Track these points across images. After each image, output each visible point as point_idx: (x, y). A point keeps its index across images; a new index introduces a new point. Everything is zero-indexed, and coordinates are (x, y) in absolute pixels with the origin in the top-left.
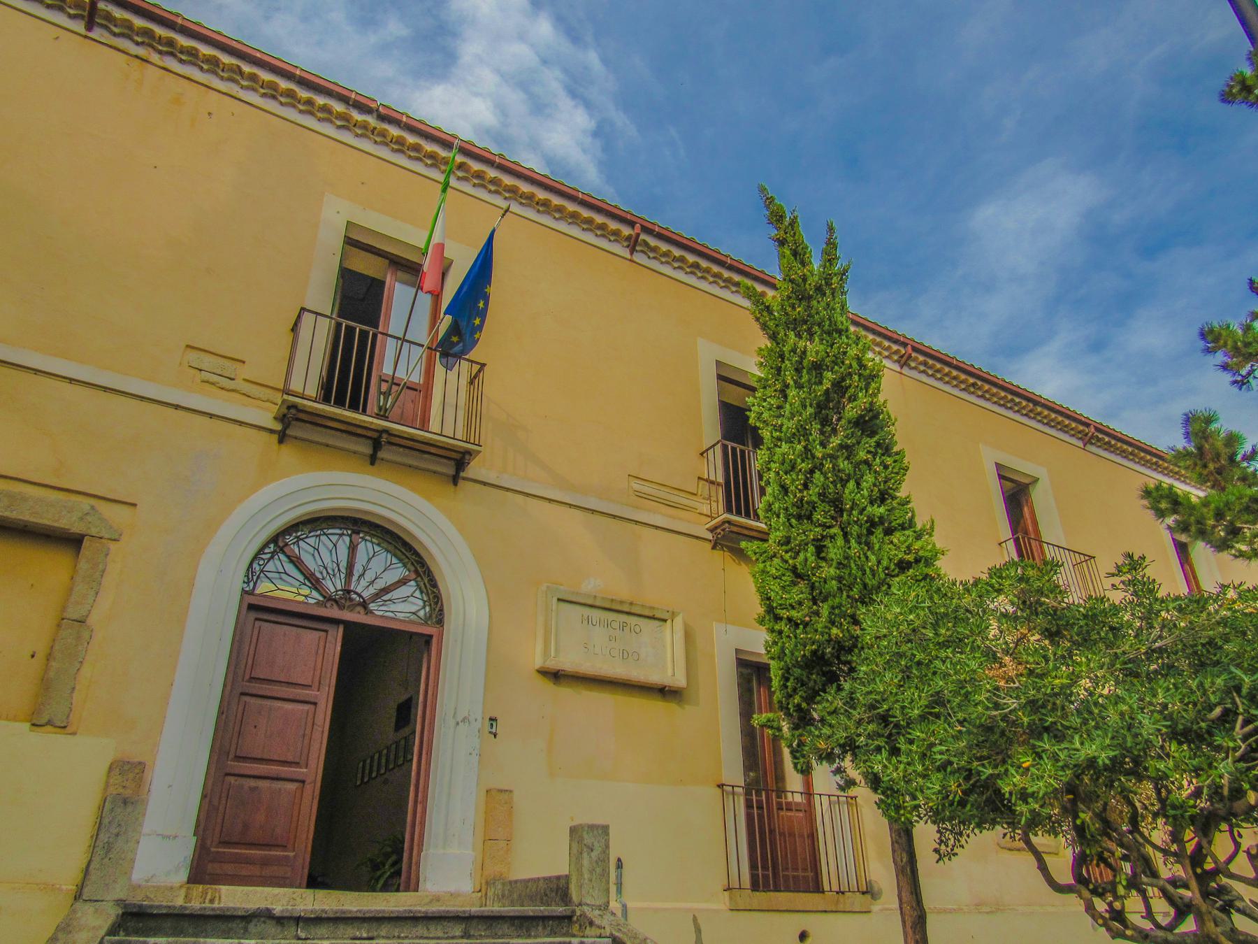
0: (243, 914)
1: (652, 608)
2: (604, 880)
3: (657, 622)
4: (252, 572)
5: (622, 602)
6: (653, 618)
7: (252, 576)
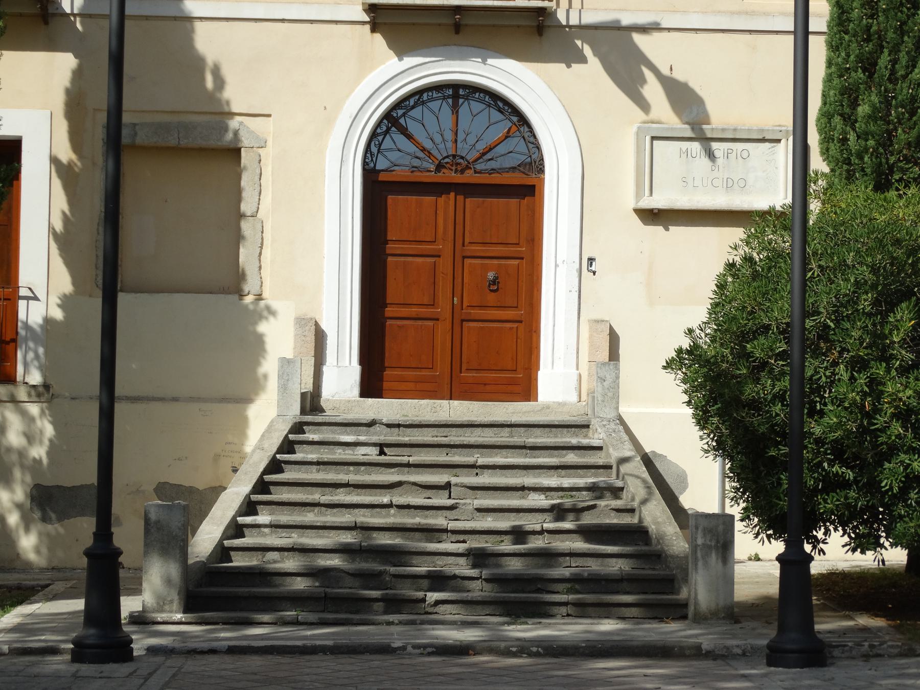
0: (366, 422)
1: (762, 130)
2: (614, 401)
3: (767, 144)
4: (371, 155)
5: (723, 130)
6: (763, 140)
7: (372, 157)
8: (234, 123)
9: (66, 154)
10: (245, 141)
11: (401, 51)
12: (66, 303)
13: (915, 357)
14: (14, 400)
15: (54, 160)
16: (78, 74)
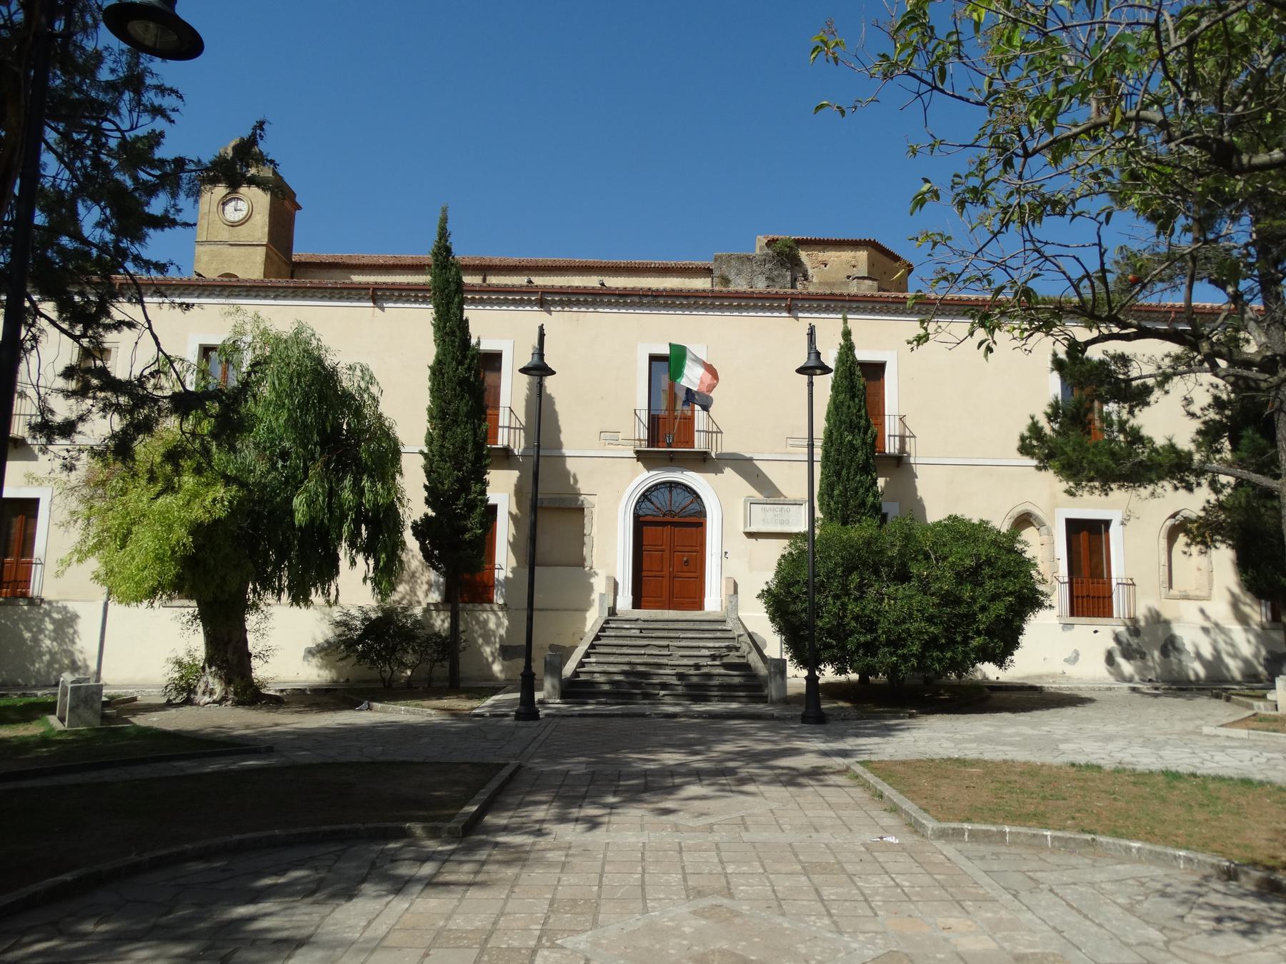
8: (582, 498)
9: (515, 511)
10: (586, 505)
11: (649, 470)
12: (514, 570)
15: (510, 513)
16: (520, 479)
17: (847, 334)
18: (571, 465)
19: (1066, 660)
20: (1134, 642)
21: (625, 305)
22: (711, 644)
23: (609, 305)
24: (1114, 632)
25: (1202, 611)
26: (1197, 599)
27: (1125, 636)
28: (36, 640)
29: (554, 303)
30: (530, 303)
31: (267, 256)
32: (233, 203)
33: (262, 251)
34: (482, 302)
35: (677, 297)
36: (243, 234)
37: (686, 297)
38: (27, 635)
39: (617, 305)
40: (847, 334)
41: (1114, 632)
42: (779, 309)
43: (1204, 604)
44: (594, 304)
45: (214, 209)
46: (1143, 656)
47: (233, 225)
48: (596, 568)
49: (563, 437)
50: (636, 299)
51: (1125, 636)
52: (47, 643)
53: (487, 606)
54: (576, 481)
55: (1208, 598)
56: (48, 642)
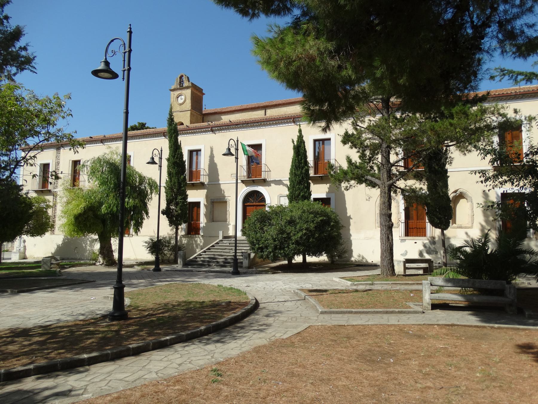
8: (226, 198)
9: (206, 203)
10: (227, 200)
11: (247, 187)
12: (206, 224)
13: (506, 203)
14: (199, 237)
15: (204, 204)
16: (207, 192)
17: (300, 131)
18: (223, 187)
19: (401, 255)
20: (432, 247)
21: (238, 128)
22: (245, 248)
23: (233, 129)
24: (423, 243)
25: (467, 233)
26: (466, 228)
27: (428, 245)
28: (86, 247)
29: (216, 130)
30: (209, 131)
31: (191, 114)
32: (180, 97)
33: (189, 112)
34: (183, 134)
35: (255, 123)
36: (184, 107)
37: (257, 122)
38: (84, 245)
39: (236, 128)
40: (300, 131)
41: (423, 243)
42: (290, 122)
43: (468, 231)
44: (228, 129)
45: (175, 100)
46: (436, 253)
47: (181, 104)
48: (230, 223)
49: (220, 177)
50: (241, 125)
51: (428, 245)
52: (88, 247)
53: (197, 236)
54: (224, 192)
55: (471, 227)
56: (88, 247)
